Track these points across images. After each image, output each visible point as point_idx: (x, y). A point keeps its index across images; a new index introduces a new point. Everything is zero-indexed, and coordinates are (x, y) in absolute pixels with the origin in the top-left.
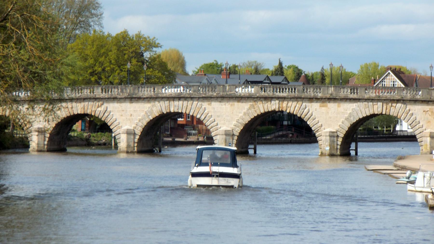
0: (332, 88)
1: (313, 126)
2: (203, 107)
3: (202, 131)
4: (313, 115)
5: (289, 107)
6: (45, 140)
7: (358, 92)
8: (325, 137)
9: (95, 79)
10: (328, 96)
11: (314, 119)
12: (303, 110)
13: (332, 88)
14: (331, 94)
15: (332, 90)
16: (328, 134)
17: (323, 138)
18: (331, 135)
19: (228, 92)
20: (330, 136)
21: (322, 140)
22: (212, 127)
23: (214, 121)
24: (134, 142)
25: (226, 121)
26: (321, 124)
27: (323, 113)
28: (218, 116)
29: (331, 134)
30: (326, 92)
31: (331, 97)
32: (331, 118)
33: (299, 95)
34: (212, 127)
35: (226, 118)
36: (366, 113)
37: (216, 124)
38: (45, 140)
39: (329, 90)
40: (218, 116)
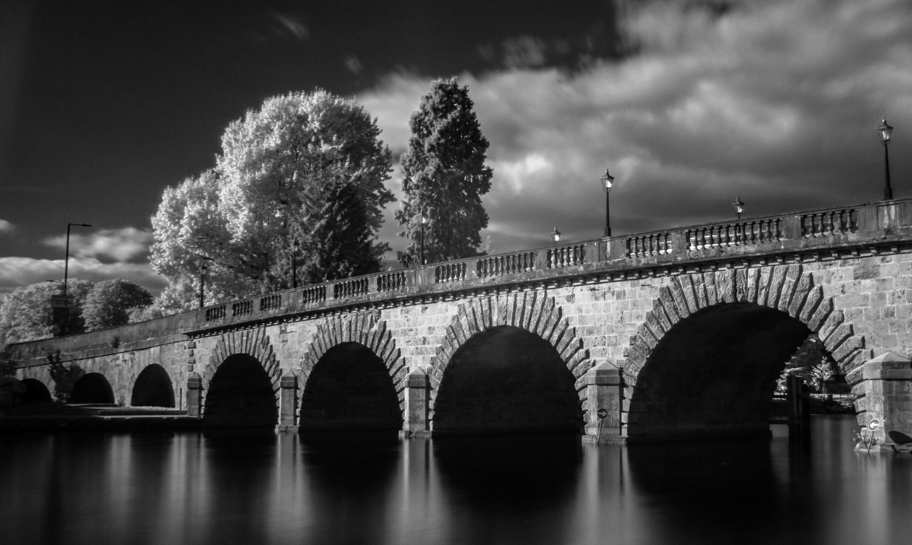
0: (893, 207)
1: (836, 347)
2: (806, 273)
3: (609, 364)
4: (836, 308)
5: (762, 289)
6: (296, 407)
7: (406, 283)
8: (871, 382)
9: (4, 303)
10: (880, 237)
11: (839, 323)
12: (803, 295)
13: (893, 207)
14: (888, 231)
15: (893, 217)
16: (878, 373)
17: (868, 387)
18: (888, 376)
19: (611, 258)
20: (887, 379)
21: (864, 395)
22: (576, 364)
23: (578, 345)
24: (428, 410)
25: (609, 345)
26: (860, 338)
27: (866, 297)
28: (590, 332)
29: (890, 373)
30: (874, 227)
31: (890, 238)
32: (892, 315)
33: (790, 247)
34: (576, 364)
35: (606, 336)
36: (593, 384)
37: (583, 356)
38: (296, 407)
39: (883, 216)
40: (590, 332)
